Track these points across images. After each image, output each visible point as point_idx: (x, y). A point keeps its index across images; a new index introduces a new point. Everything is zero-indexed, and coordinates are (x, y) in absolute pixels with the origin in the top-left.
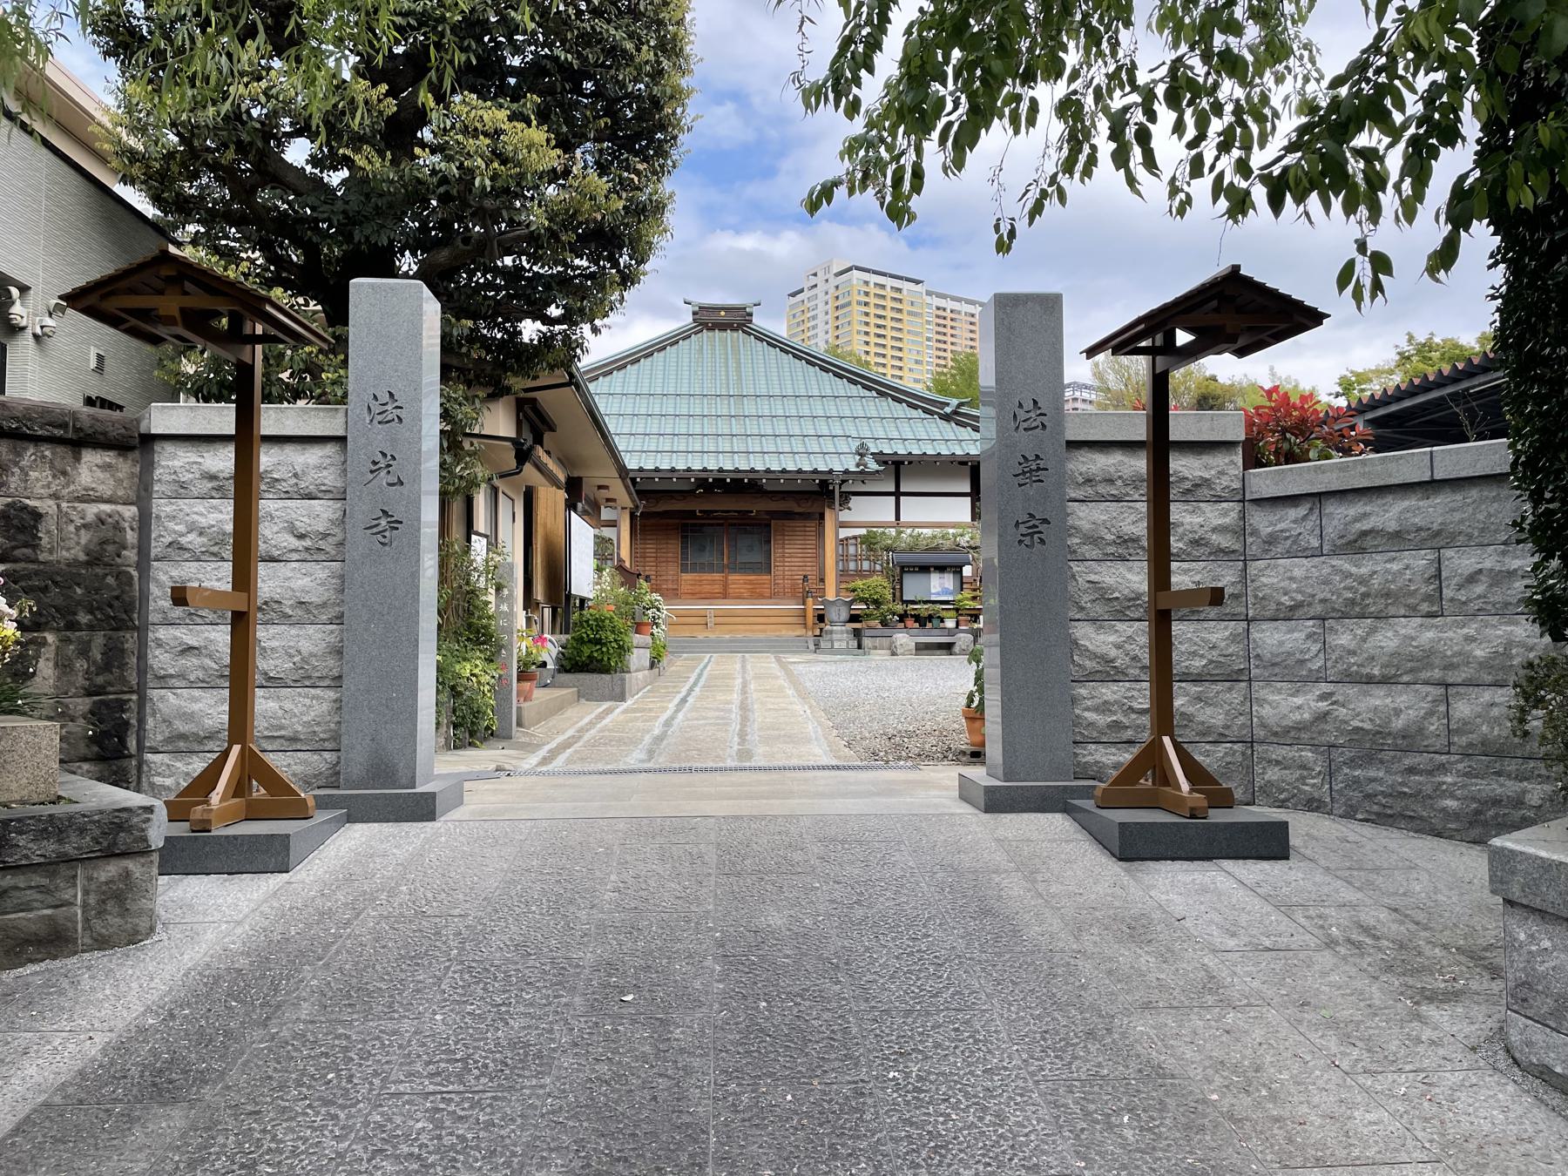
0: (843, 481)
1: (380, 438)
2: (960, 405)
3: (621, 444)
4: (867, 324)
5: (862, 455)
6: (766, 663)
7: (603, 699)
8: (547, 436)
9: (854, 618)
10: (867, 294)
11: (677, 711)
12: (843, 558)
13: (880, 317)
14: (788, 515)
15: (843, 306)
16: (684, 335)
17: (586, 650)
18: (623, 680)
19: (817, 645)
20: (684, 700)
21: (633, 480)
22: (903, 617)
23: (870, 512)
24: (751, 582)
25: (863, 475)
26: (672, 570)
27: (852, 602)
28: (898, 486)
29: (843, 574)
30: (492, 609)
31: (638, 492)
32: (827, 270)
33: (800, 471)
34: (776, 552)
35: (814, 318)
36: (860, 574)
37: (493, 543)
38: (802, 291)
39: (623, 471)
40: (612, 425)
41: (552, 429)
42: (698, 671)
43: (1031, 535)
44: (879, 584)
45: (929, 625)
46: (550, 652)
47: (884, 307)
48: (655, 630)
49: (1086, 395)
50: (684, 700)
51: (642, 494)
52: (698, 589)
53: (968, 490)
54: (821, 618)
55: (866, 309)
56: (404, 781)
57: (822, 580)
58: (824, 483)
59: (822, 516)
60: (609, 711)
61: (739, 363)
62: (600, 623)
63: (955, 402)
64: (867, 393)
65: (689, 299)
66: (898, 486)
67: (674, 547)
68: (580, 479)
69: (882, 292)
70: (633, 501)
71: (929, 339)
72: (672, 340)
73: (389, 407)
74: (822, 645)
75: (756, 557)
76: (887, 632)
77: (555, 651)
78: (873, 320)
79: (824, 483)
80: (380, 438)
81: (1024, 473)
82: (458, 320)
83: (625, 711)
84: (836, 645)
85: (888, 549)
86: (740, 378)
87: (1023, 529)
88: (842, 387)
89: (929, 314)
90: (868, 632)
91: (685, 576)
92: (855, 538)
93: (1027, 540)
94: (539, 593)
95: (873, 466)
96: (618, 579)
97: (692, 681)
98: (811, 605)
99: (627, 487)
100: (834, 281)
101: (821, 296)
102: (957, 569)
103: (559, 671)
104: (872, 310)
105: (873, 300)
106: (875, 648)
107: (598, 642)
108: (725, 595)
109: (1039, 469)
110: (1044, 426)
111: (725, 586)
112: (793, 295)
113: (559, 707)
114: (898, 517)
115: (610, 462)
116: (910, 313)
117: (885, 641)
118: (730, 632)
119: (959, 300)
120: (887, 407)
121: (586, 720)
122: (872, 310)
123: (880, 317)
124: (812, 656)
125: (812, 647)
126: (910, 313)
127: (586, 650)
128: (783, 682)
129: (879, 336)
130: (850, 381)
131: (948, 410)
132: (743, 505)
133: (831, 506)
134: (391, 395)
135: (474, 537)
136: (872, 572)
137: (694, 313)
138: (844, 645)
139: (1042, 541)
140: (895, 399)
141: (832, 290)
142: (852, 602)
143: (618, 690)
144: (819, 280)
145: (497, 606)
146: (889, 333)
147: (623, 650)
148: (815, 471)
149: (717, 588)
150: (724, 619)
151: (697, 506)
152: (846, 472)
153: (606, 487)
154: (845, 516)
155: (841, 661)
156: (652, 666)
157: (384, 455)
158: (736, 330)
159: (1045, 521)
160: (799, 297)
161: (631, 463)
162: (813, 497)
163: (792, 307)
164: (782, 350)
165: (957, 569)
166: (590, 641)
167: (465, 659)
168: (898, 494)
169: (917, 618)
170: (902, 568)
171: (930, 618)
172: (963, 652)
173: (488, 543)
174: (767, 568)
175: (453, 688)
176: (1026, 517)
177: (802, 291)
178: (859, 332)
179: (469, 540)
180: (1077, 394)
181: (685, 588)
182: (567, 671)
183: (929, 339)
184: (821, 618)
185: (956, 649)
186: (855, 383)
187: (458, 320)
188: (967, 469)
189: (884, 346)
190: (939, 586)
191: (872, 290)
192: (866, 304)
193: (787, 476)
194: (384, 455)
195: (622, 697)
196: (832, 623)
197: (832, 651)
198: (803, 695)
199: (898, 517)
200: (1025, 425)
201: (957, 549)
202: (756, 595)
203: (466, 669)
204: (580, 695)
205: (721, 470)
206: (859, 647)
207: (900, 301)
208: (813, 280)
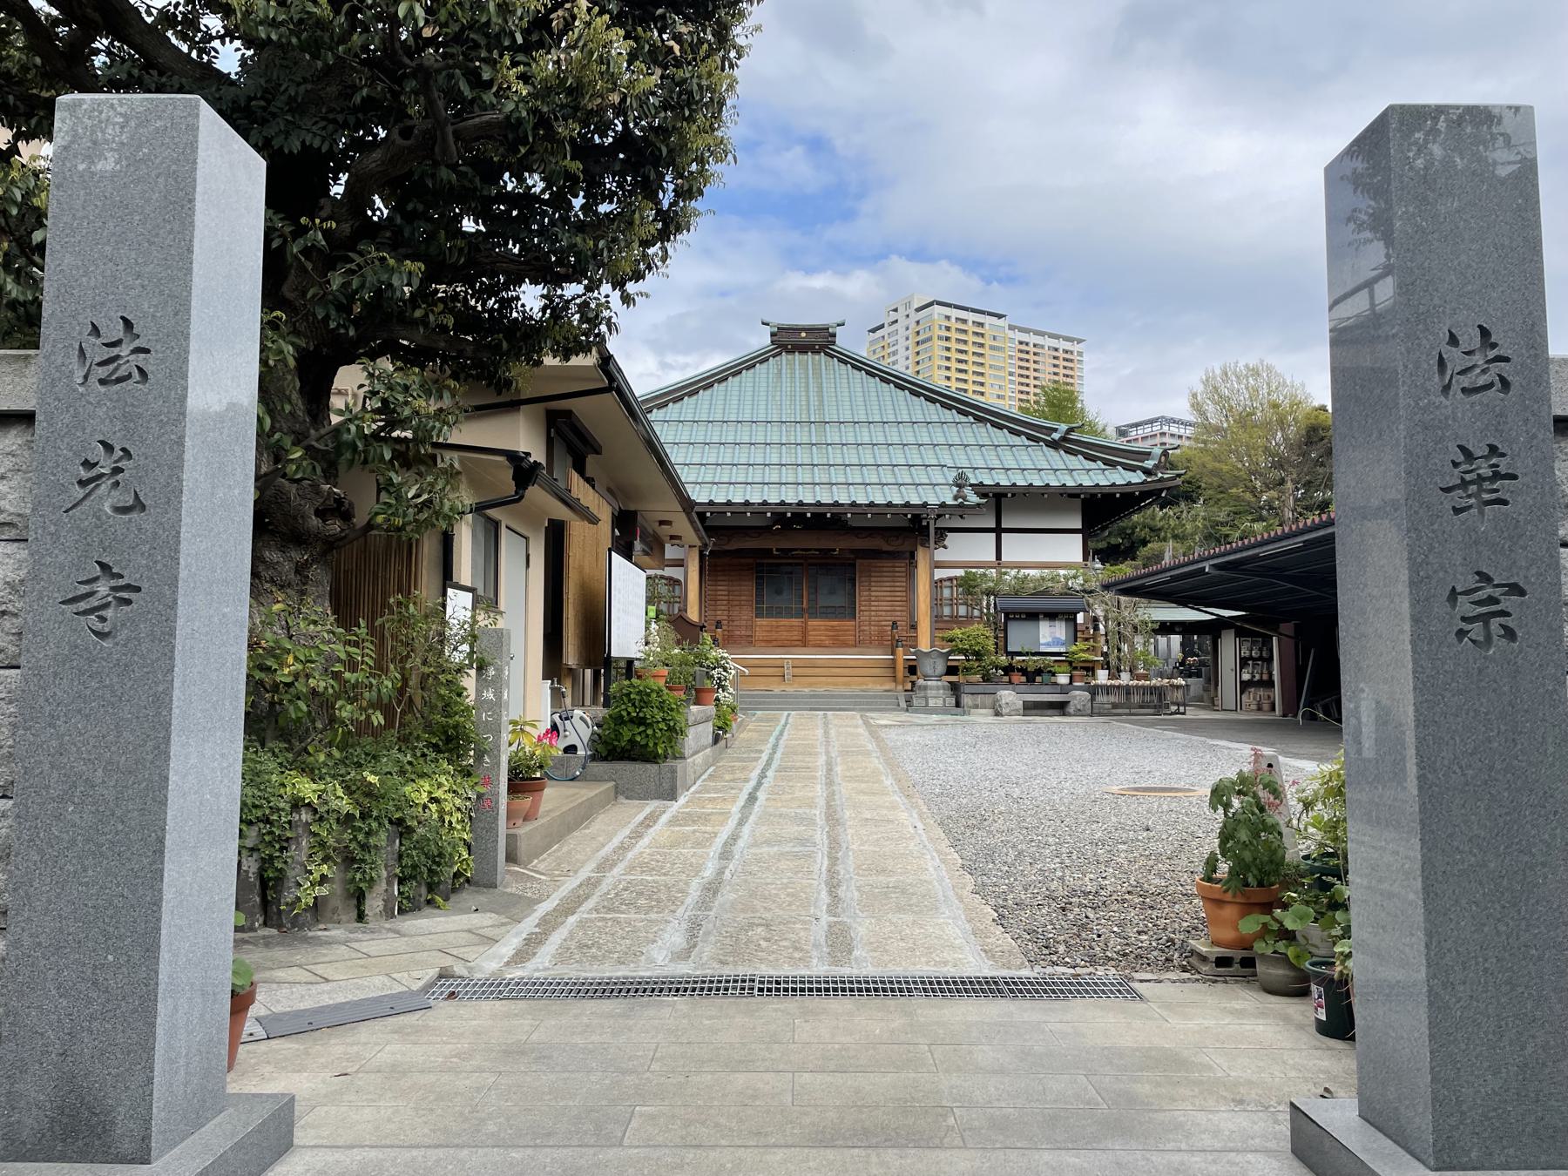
0: (939, 516)
1: (101, 415)
2: (1071, 430)
3: (685, 475)
4: (948, 359)
5: (960, 486)
6: (848, 726)
7: (646, 796)
8: (591, 460)
9: (952, 671)
10: (948, 329)
11: (741, 823)
12: (937, 602)
13: (961, 351)
14: (876, 554)
15: (924, 342)
17: (626, 733)
18: (674, 771)
19: (909, 701)
20: (752, 798)
21: (701, 516)
22: (1008, 670)
23: (968, 550)
24: (833, 628)
25: (961, 509)
26: (745, 615)
27: (949, 653)
28: (998, 522)
29: (938, 621)
30: (471, 697)
31: (706, 529)
32: (908, 305)
33: (890, 505)
34: (862, 595)
35: (895, 353)
36: (955, 620)
37: (486, 600)
38: (882, 326)
39: (688, 504)
40: (675, 456)
41: (597, 451)
42: (772, 740)
43: (1485, 618)
44: (980, 633)
45: (1038, 679)
46: (580, 730)
47: (965, 342)
48: (721, 695)
49: (1174, 430)
50: (752, 798)
51: (711, 530)
52: (774, 635)
53: (1079, 526)
54: (912, 670)
55: (948, 344)
56: (127, 1147)
57: (914, 627)
58: (917, 518)
59: (912, 555)
60: (651, 820)
61: (820, 387)
62: (644, 698)
63: (1064, 427)
64: (963, 419)
66: (998, 522)
67: (747, 589)
68: (635, 513)
69: (963, 327)
70: (700, 538)
71: (1011, 374)
72: (749, 364)
73: (124, 350)
74: (915, 702)
75: (839, 600)
76: (989, 688)
77: (586, 733)
78: (954, 355)
79: (917, 518)
80: (101, 415)
81: (1464, 484)
82: (400, 261)
83: (674, 821)
84: (932, 703)
85: (988, 593)
86: (821, 402)
87: (1465, 606)
88: (934, 412)
89: (1012, 349)
90: (968, 689)
91: (759, 621)
92: (950, 579)
93: (1476, 630)
94: (571, 657)
95: (973, 499)
96: (673, 636)
97: (765, 757)
98: (902, 655)
99: (692, 522)
100: (915, 317)
101: (902, 332)
102: (1070, 617)
103: (593, 758)
104: (954, 345)
105: (954, 335)
106: (976, 707)
107: (641, 721)
108: (804, 643)
109: (1497, 476)
110: (1505, 384)
111: (805, 632)
112: (873, 331)
113: (582, 816)
114: (999, 556)
115: (670, 493)
116: (992, 348)
117: (988, 699)
118: (810, 685)
119: (1042, 334)
120: (985, 433)
121: (616, 841)
122: (954, 345)
123: (961, 351)
124: (905, 717)
125: (903, 705)
126: (992, 348)
127: (626, 733)
128: (876, 763)
129: (961, 371)
130: (944, 405)
131: (1056, 436)
132: (825, 543)
133: (925, 543)
134: (128, 324)
135: (450, 591)
136: (969, 619)
137: (773, 335)
138: (940, 702)
139: (1510, 634)
140: (994, 425)
141: (913, 326)
142: (949, 653)
143: (666, 786)
144: (900, 315)
145: (479, 692)
146: (971, 368)
147: (674, 732)
148: (907, 505)
149: (796, 635)
151: (773, 544)
152: (943, 505)
153: (668, 523)
154: (940, 555)
155: (941, 724)
156: (716, 739)
157: (108, 448)
158: (818, 352)
159: (1516, 590)
160: (879, 333)
161: (699, 495)
162: (903, 534)
163: (872, 343)
164: (868, 373)
165: (1070, 617)
166: (632, 721)
167: (423, 775)
168: (998, 531)
169: (1023, 671)
170: (1007, 615)
171: (1039, 672)
172: (1079, 713)
173: (476, 602)
174: (850, 612)
175: (400, 822)
176: (1472, 581)
177: (882, 326)
178: (939, 367)
179: (444, 594)
180: (1165, 428)
181: (759, 634)
182: (605, 759)
183: (1011, 374)
184: (912, 670)
185: (1071, 709)
186: (950, 408)
187: (400, 261)
188: (1078, 502)
189: (965, 381)
190: (1050, 635)
191: (953, 324)
192: (947, 339)
193: (875, 510)
194: (108, 448)
195: (672, 796)
196: (926, 677)
197: (927, 710)
198: (908, 789)
199: (999, 556)
200: (1465, 381)
201: (1068, 593)
202: (839, 644)
203: (420, 792)
204: (618, 791)
205: (801, 504)
206: (958, 705)
207: (982, 335)
208: (893, 316)
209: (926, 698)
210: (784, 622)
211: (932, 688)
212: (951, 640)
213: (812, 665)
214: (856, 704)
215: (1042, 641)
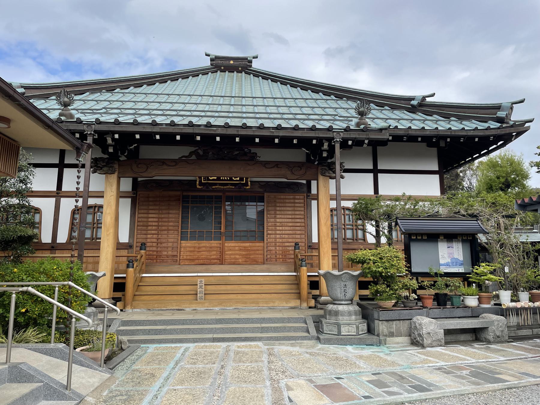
16: (204, 72)
19: (319, 329)
24: (245, 249)
28: (375, 164)
53: (436, 168)
65: (208, 52)
66: (375, 164)
67: (174, 217)
76: (406, 313)
84: (344, 330)
91: (184, 243)
98: (305, 272)
106: (392, 335)
111: (222, 252)
117: (404, 326)
138: (353, 331)
149: (214, 255)
150: (216, 291)
168: (375, 171)
172: (499, 340)
181: (184, 254)
184: (314, 285)
190: (450, 257)
193: (281, 133)
202: (250, 261)
206: (370, 330)
209: (339, 326)
210: (205, 243)
211: (343, 314)
212: (363, 262)
213: (225, 282)
214: (263, 330)
215: (442, 261)
